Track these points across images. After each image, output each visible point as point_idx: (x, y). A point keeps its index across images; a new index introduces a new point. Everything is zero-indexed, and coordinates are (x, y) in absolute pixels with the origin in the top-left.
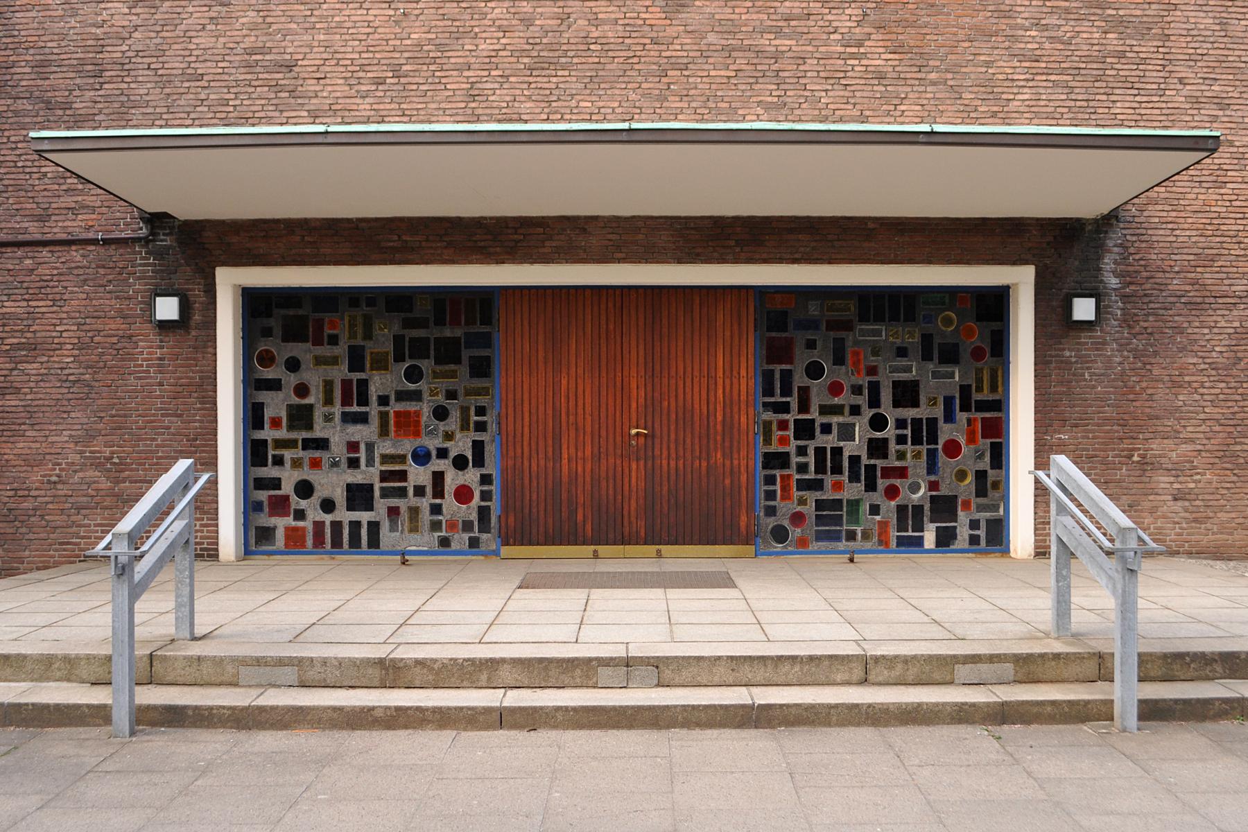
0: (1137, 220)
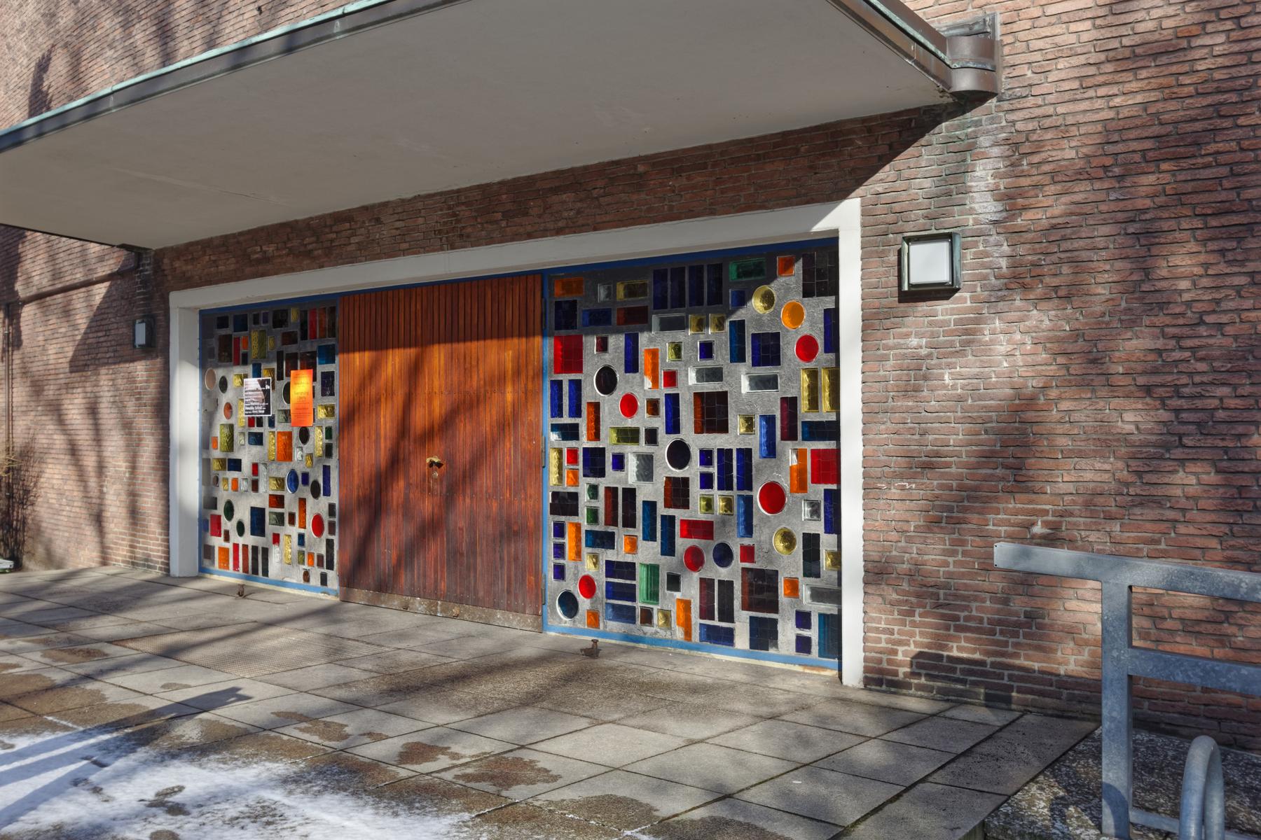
0: (1035, 91)
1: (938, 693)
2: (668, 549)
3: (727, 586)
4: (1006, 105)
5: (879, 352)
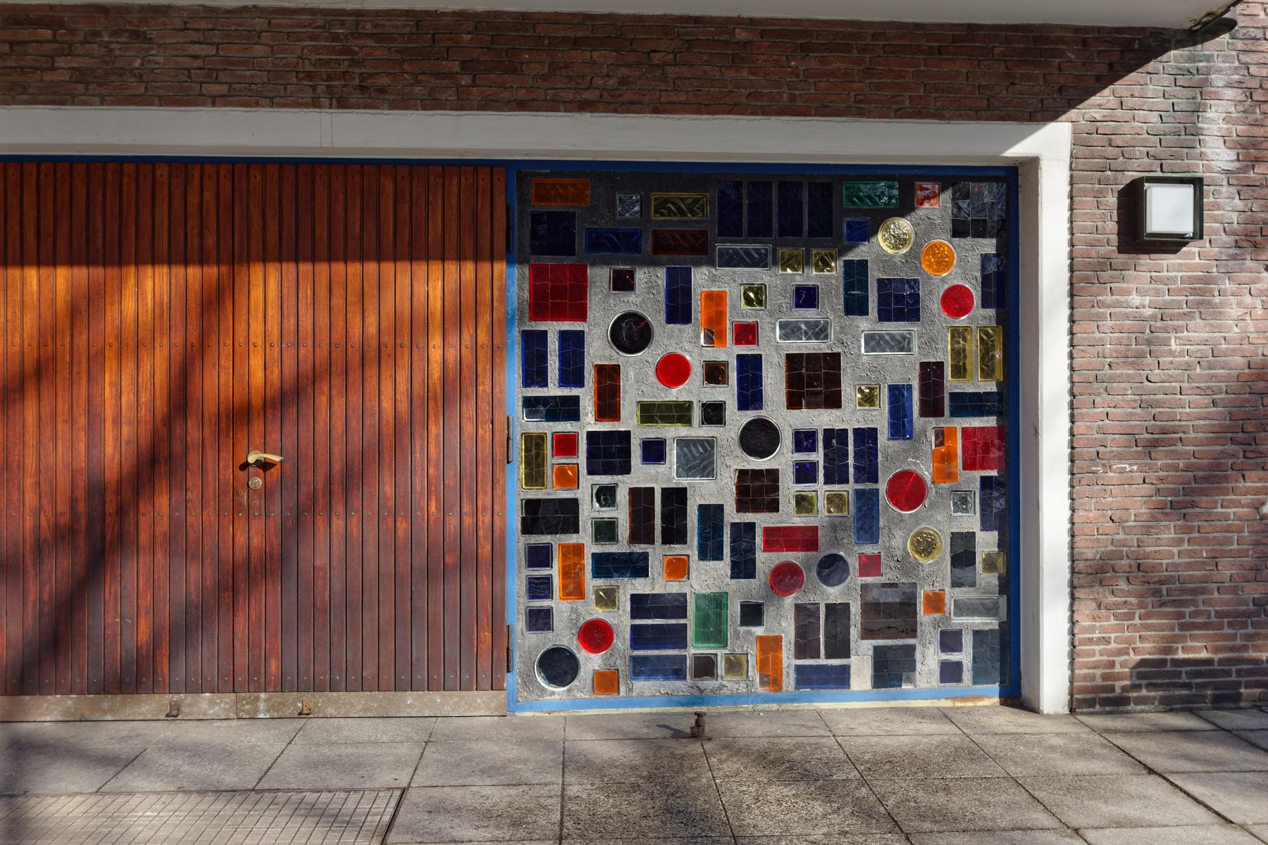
1: (1160, 703)
2: (744, 567)
3: (838, 612)
4: (1240, 45)
5: (1093, 311)
